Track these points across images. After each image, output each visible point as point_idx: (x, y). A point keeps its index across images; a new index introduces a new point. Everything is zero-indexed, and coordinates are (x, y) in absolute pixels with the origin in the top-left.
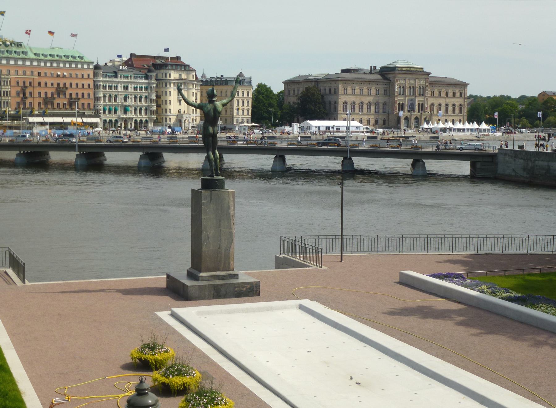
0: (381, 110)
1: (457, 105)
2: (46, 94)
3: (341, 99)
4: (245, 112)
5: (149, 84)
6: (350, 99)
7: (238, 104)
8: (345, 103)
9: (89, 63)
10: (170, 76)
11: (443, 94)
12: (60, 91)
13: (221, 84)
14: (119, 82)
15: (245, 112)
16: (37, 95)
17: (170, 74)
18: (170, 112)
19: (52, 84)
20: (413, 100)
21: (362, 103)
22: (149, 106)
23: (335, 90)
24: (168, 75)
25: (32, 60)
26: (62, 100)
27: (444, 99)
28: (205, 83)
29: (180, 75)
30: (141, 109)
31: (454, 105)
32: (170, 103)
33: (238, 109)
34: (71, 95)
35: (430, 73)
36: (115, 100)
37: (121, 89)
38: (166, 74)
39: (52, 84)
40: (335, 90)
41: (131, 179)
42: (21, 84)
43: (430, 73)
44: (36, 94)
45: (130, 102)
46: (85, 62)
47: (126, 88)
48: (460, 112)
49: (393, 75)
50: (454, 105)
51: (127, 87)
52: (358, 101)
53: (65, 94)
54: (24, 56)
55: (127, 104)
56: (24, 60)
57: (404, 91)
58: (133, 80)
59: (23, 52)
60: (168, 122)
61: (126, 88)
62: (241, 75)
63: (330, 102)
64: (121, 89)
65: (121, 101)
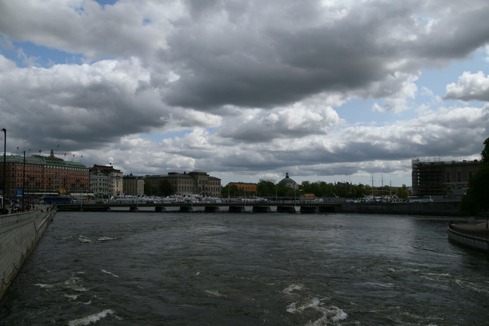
0: (192, 190)
1: (217, 188)
2: (72, 182)
3: (179, 185)
4: (142, 191)
5: (108, 178)
6: (181, 185)
7: (139, 187)
8: (180, 187)
9: (87, 169)
10: (114, 175)
11: (184, 182)
12: (78, 181)
13: (131, 179)
14: (98, 177)
15: (142, 191)
16: (69, 183)
17: (114, 174)
18: (114, 191)
19: (74, 178)
20: (204, 186)
21: (186, 187)
22: (108, 188)
23: (176, 181)
24: (113, 174)
25: (68, 167)
26: (32, 184)
27: (184, 184)
28: (126, 178)
29: (117, 175)
30: (105, 189)
31: (216, 188)
32: (114, 187)
33: (141, 189)
34: (36, 180)
35: (209, 175)
36: (96, 185)
37: (98, 180)
38: (113, 174)
39: (74, 178)
40: (176, 181)
41: (177, 214)
42: (63, 178)
43: (209, 175)
44: (68, 183)
45: (102, 186)
46: (86, 168)
47: (100, 180)
48: (219, 191)
49: (197, 176)
50: (188, 187)
51: (101, 179)
52: (184, 186)
53: (34, 180)
54: (84, 167)
55: (101, 187)
56: (65, 167)
57: (201, 182)
58: (103, 177)
59: (64, 163)
60: (113, 195)
61: (100, 180)
62: (131, 174)
63: (173, 187)
64: (98, 180)
65: (98, 186)
